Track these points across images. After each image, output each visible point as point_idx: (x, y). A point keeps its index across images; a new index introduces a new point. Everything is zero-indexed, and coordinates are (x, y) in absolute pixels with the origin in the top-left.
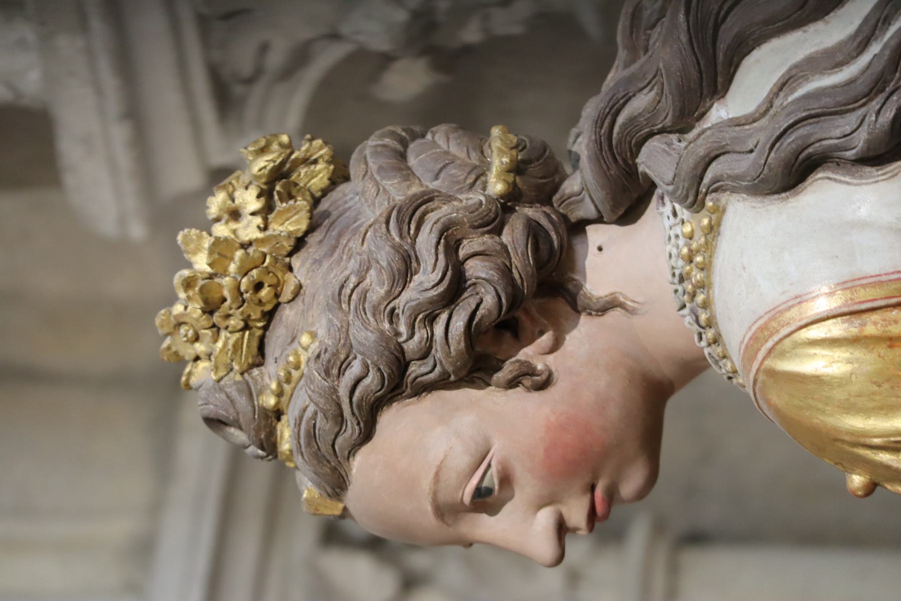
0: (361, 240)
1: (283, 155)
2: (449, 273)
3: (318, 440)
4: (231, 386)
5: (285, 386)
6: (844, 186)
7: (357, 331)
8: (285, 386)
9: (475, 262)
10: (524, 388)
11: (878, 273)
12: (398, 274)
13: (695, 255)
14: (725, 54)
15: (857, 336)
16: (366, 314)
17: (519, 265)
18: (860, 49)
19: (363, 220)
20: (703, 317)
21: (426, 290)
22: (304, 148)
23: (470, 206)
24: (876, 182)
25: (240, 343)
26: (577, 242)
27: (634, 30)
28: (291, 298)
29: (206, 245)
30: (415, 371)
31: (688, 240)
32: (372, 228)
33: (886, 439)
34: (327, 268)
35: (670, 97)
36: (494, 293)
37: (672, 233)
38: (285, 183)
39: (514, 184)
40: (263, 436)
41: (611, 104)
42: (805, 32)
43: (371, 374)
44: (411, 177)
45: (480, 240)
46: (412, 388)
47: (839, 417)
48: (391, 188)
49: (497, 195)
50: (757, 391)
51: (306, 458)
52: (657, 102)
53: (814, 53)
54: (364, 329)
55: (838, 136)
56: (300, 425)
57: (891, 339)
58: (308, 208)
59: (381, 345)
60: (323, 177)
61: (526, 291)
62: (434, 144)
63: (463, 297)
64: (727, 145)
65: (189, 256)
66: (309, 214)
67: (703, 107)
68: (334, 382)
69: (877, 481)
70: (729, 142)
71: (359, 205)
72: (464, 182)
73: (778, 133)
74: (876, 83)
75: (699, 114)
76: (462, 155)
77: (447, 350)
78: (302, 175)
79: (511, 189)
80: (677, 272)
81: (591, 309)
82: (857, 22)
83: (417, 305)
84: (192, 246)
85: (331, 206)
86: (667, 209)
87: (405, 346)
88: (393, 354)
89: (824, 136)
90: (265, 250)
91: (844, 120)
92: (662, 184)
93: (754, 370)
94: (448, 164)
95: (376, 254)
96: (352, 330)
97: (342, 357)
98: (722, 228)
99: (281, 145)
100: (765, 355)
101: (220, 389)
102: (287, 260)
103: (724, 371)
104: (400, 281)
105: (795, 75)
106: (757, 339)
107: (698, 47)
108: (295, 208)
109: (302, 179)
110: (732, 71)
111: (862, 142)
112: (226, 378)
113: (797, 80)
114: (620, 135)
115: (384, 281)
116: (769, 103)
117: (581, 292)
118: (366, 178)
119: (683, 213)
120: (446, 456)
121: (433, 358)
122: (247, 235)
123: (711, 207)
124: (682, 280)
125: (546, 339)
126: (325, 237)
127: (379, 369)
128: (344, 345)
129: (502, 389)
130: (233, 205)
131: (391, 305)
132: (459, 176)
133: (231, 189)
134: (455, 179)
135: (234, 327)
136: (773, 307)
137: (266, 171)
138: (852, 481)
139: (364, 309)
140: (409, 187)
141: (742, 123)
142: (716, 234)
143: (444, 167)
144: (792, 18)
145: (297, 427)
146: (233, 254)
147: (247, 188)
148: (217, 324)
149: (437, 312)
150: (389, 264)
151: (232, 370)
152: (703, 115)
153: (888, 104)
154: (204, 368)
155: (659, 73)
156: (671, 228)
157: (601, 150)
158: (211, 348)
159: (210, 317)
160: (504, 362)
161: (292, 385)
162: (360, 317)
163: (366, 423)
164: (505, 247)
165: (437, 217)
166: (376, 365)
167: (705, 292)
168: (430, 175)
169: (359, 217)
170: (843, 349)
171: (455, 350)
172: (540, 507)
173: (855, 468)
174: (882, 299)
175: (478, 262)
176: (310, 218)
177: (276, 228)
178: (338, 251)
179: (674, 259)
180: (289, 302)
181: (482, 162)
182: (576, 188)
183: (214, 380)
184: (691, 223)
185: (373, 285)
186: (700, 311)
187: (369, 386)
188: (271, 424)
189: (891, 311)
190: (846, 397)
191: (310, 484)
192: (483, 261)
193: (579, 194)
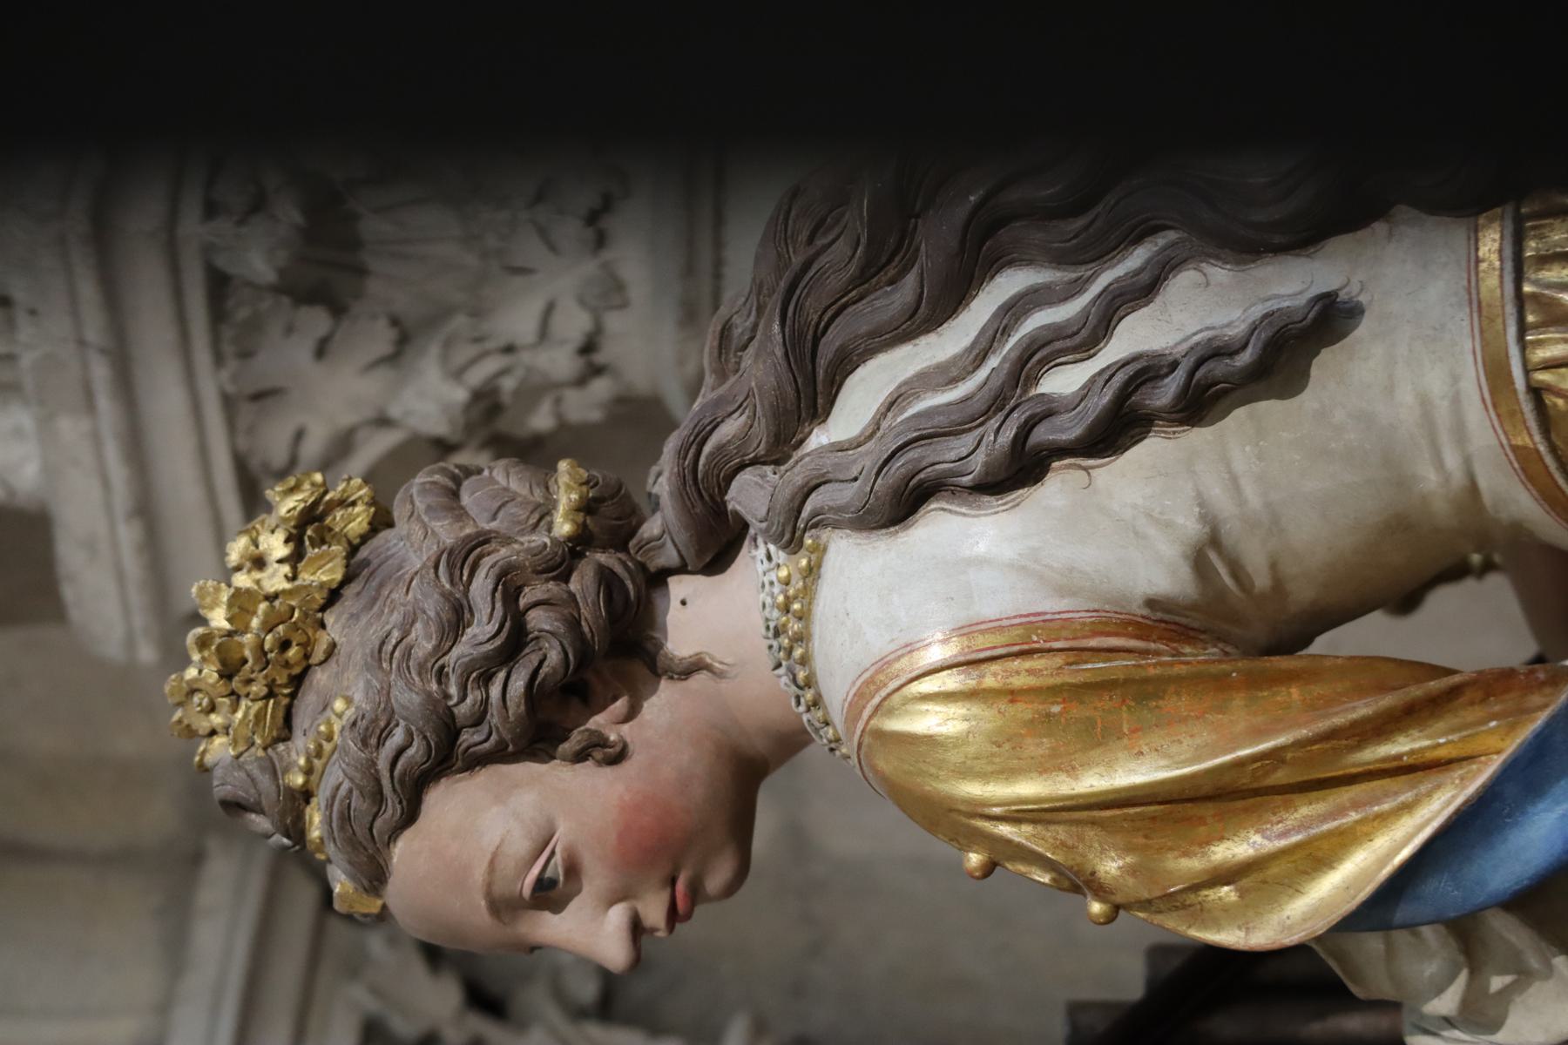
0: (405, 590)
1: (316, 494)
2: (508, 624)
3: (353, 824)
4: (252, 763)
5: (316, 761)
6: (959, 518)
7: (400, 692)
8: (316, 761)
9: (537, 612)
10: (593, 761)
11: (998, 617)
12: (449, 626)
13: (792, 603)
14: (826, 371)
15: (974, 688)
16: (410, 673)
17: (589, 617)
18: (977, 362)
19: (407, 568)
20: (801, 675)
21: (481, 644)
22: (340, 488)
23: (533, 548)
24: (996, 513)
25: (263, 714)
26: (657, 597)
27: (723, 351)
28: (322, 659)
29: (225, 599)
30: (467, 739)
31: (784, 587)
32: (419, 575)
33: (1007, 808)
34: (367, 623)
35: (763, 421)
36: (559, 648)
37: (766, 580)
38: (318, 528)
39: (584, 525)
40: (288, 821)
41: (696, 431)
42: (915, 345)
43: (415, 743)
44: (464, 518)
45: (544, 587)
46: (463, 760)
47: (954, 783)
48: (441, 530)
49: (564, 537)
50: (862, 756)
51: (338, 844)
52: (748, 426)
53: (926, 368)
54: (407, 691)
55: (953, 459)
56: (332, 805)
57: (1012, 692)
58: (344, 554)
59: (428, 709)
60: (363, 520)
61: (597, 647)
62: (491, 480)
63: (523, 654)
64: (828, 472)
65: (205, 611)
66: (345, 561)
67: (801, 432)
68: (372, 753)
69: (996, 860)
70: (830, 469)
71: (404, 551)
72: (526, 522)
73: (885, 456)
74: (995, 400)
75: (796, 441)
76: (524, 491)
77: (505, 714)
78: (338, 518)
79: (580, 532)
80: (772, 625)
81: (673, 672)
82: (973, 334)
83: (471, 661)
84: (208, 600)
85: (371, 553)
86: (761, 553)
87: (456, 710)
88: (441, 719)
89: (937, 459)
90: (293, 603)
91: (959, 441)
92: (754, 521)
93: (858, 732)
94: (507, 502)
95: (422, 602)
96: (395, 692)
97: (382, 724)
98: (823, 570)
99: (313, 484)
100: (870, 713)
101: (239, 766)
102: (320, 615)
103: (825, 741)
104: (451, 634)
105: (905, 392)
106: (861, 696)
107: (796, 361)
108: (329, 555)
109: (337, 523)
110: (834, 392)
111: (979, 465)
112: (246, 754)
113: (908, 398)
114: (707, 467)
115: (432, 635)
116: (876, 424)
117: (662, 652)
118: (412, 519)
119: (780, 556)
120: (502, 841)
121: (488, 727)
122: (272, 586)
123: (810, 546)
124: (777, 634)
125: (620, 705)
126: (363, 588)
127: (425, 737)
128: (385, 709)
129: (568, 763)
130: (257, 552)
131: (440, 662)
132: (520, 515)
133: (254, 534)
134: (515, 519)
135: (256, 694)
136: (880, 658)
137: (296, 513)
138: (968, 861)
139: (408, 668)
140: (462, 528)
141: (845, 447)
142: (816, 577)
143: (503, 505)
144: (900, 330)
145: (329, 809)
146: (257, 608)
147: (273, 532)
148: (236, 690)
149: (493, 670)
150: (438, 614)
151: (253, 744)
152: (802, 442)
153: (1007, 422)
154: (221, 744)
155: (751, 393)
156: (765, 574)
157: (685, 484)
158: (230, 719)
159: (228, 682)
160: (572, 730)
161: (324, 760)
162: (403, 676)
163: (409, 801)
164: (572, 596)
165: (495, 560)
166: (422, 733)
167: (804, 645)
168: (486, 515)
169: (404, 564)
170: (960, 704)
171: (513, 714)
172: (611, 903)
173: (972, 845)
174: (1002, 646)
175: (541, 613)
176: (347, 566)
177: (306, 577)
178: (379, 603)
179: (768, 609)
180: (321, 663)
181: (547, 499)
182: (656, 531)
183: (233, 757)
184: (787, 567)
185: (420, 640)
186: (798, 667)
187: (413, 756)
188: (298, 807)
189: (1013, 661)
190: (963, 760)
191: (343, 877)
192: (546, 611)
193: (660, 539)
